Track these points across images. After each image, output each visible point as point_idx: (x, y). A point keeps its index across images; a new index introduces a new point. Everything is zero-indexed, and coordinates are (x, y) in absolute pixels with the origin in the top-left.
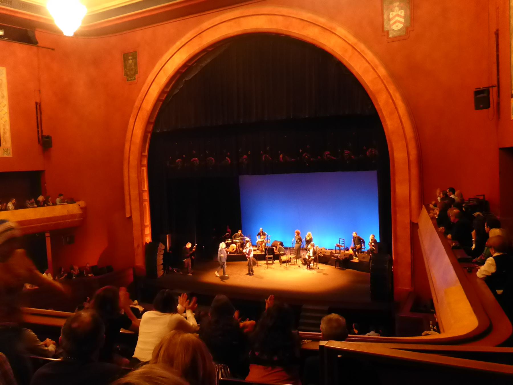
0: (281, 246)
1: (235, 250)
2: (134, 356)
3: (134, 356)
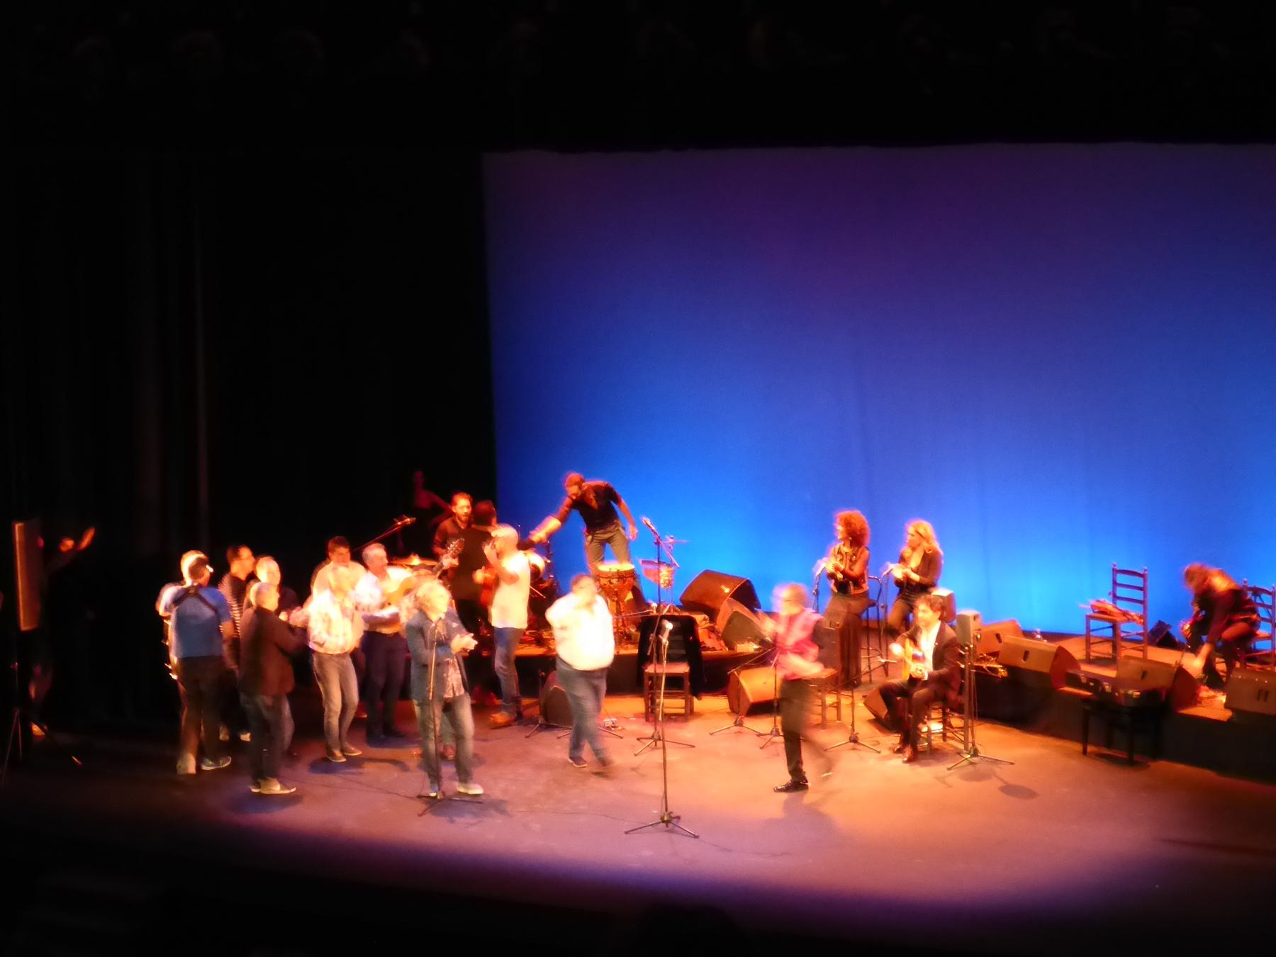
0: (744, 611)
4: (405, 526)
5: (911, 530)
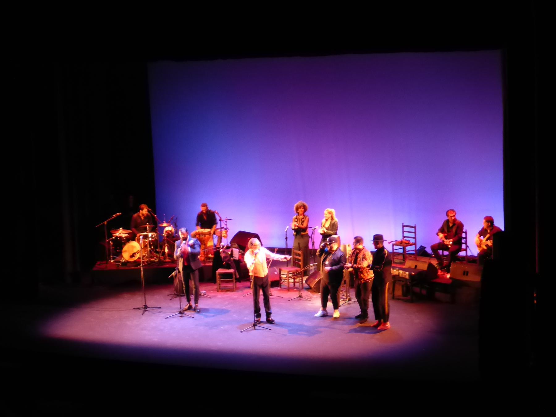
1: (138, 256)
2: (503, 229)
3: (503, 229)
4: (118, 216)
5: (326, 212)
